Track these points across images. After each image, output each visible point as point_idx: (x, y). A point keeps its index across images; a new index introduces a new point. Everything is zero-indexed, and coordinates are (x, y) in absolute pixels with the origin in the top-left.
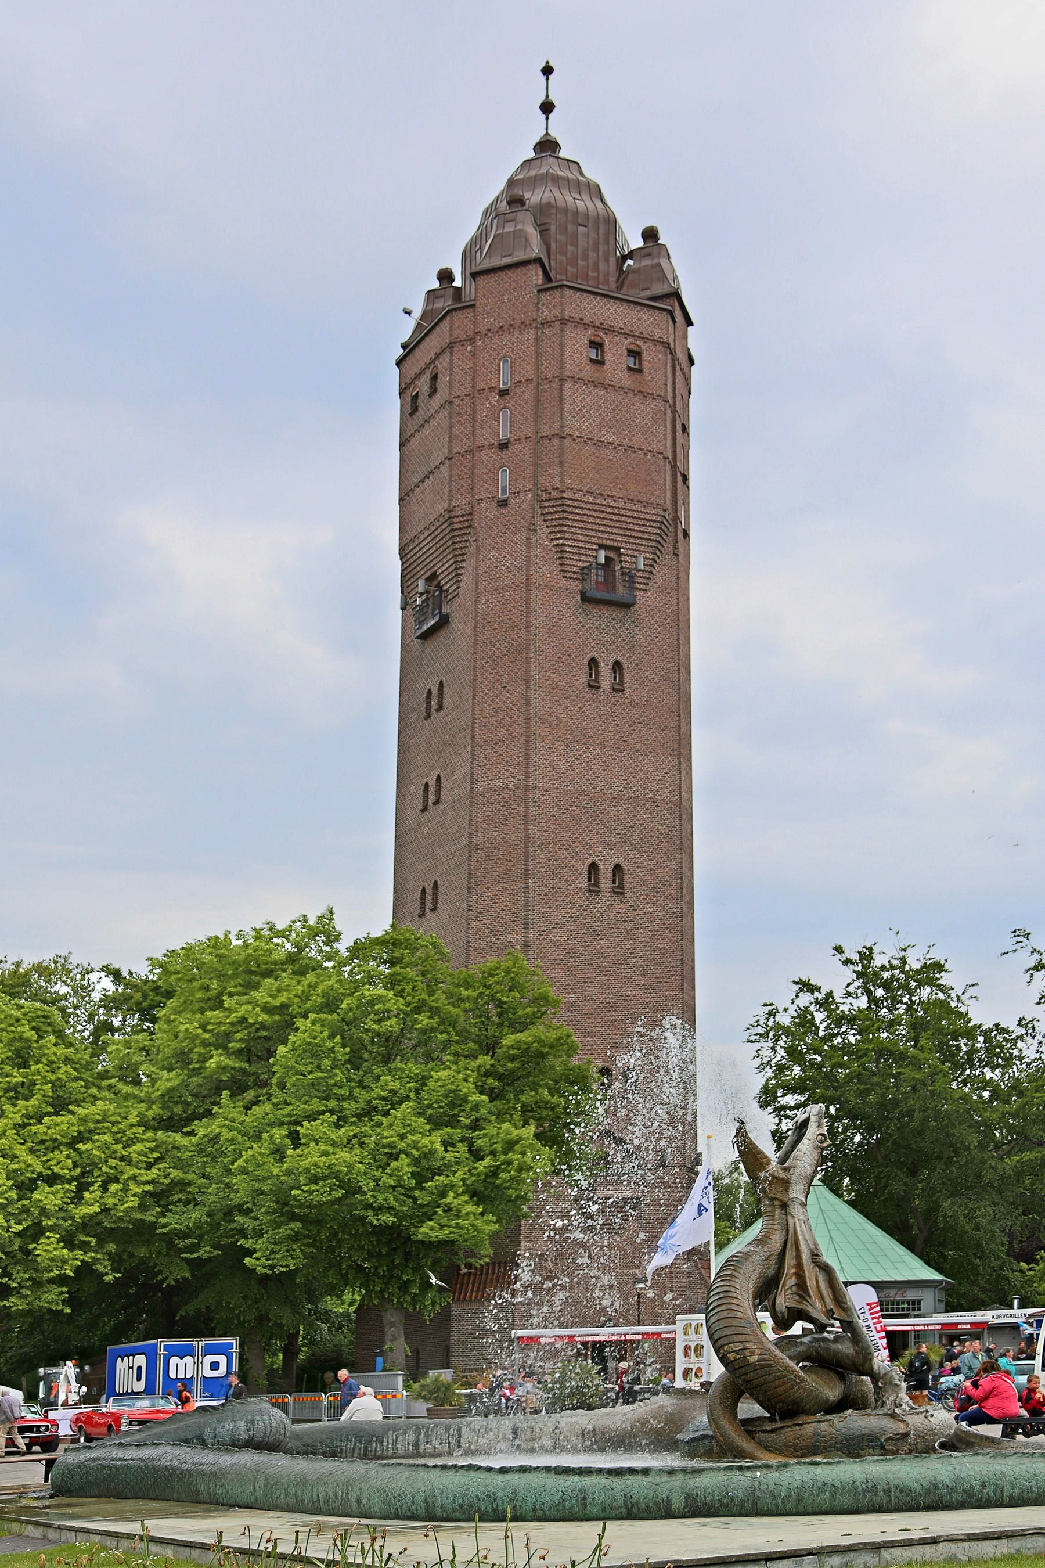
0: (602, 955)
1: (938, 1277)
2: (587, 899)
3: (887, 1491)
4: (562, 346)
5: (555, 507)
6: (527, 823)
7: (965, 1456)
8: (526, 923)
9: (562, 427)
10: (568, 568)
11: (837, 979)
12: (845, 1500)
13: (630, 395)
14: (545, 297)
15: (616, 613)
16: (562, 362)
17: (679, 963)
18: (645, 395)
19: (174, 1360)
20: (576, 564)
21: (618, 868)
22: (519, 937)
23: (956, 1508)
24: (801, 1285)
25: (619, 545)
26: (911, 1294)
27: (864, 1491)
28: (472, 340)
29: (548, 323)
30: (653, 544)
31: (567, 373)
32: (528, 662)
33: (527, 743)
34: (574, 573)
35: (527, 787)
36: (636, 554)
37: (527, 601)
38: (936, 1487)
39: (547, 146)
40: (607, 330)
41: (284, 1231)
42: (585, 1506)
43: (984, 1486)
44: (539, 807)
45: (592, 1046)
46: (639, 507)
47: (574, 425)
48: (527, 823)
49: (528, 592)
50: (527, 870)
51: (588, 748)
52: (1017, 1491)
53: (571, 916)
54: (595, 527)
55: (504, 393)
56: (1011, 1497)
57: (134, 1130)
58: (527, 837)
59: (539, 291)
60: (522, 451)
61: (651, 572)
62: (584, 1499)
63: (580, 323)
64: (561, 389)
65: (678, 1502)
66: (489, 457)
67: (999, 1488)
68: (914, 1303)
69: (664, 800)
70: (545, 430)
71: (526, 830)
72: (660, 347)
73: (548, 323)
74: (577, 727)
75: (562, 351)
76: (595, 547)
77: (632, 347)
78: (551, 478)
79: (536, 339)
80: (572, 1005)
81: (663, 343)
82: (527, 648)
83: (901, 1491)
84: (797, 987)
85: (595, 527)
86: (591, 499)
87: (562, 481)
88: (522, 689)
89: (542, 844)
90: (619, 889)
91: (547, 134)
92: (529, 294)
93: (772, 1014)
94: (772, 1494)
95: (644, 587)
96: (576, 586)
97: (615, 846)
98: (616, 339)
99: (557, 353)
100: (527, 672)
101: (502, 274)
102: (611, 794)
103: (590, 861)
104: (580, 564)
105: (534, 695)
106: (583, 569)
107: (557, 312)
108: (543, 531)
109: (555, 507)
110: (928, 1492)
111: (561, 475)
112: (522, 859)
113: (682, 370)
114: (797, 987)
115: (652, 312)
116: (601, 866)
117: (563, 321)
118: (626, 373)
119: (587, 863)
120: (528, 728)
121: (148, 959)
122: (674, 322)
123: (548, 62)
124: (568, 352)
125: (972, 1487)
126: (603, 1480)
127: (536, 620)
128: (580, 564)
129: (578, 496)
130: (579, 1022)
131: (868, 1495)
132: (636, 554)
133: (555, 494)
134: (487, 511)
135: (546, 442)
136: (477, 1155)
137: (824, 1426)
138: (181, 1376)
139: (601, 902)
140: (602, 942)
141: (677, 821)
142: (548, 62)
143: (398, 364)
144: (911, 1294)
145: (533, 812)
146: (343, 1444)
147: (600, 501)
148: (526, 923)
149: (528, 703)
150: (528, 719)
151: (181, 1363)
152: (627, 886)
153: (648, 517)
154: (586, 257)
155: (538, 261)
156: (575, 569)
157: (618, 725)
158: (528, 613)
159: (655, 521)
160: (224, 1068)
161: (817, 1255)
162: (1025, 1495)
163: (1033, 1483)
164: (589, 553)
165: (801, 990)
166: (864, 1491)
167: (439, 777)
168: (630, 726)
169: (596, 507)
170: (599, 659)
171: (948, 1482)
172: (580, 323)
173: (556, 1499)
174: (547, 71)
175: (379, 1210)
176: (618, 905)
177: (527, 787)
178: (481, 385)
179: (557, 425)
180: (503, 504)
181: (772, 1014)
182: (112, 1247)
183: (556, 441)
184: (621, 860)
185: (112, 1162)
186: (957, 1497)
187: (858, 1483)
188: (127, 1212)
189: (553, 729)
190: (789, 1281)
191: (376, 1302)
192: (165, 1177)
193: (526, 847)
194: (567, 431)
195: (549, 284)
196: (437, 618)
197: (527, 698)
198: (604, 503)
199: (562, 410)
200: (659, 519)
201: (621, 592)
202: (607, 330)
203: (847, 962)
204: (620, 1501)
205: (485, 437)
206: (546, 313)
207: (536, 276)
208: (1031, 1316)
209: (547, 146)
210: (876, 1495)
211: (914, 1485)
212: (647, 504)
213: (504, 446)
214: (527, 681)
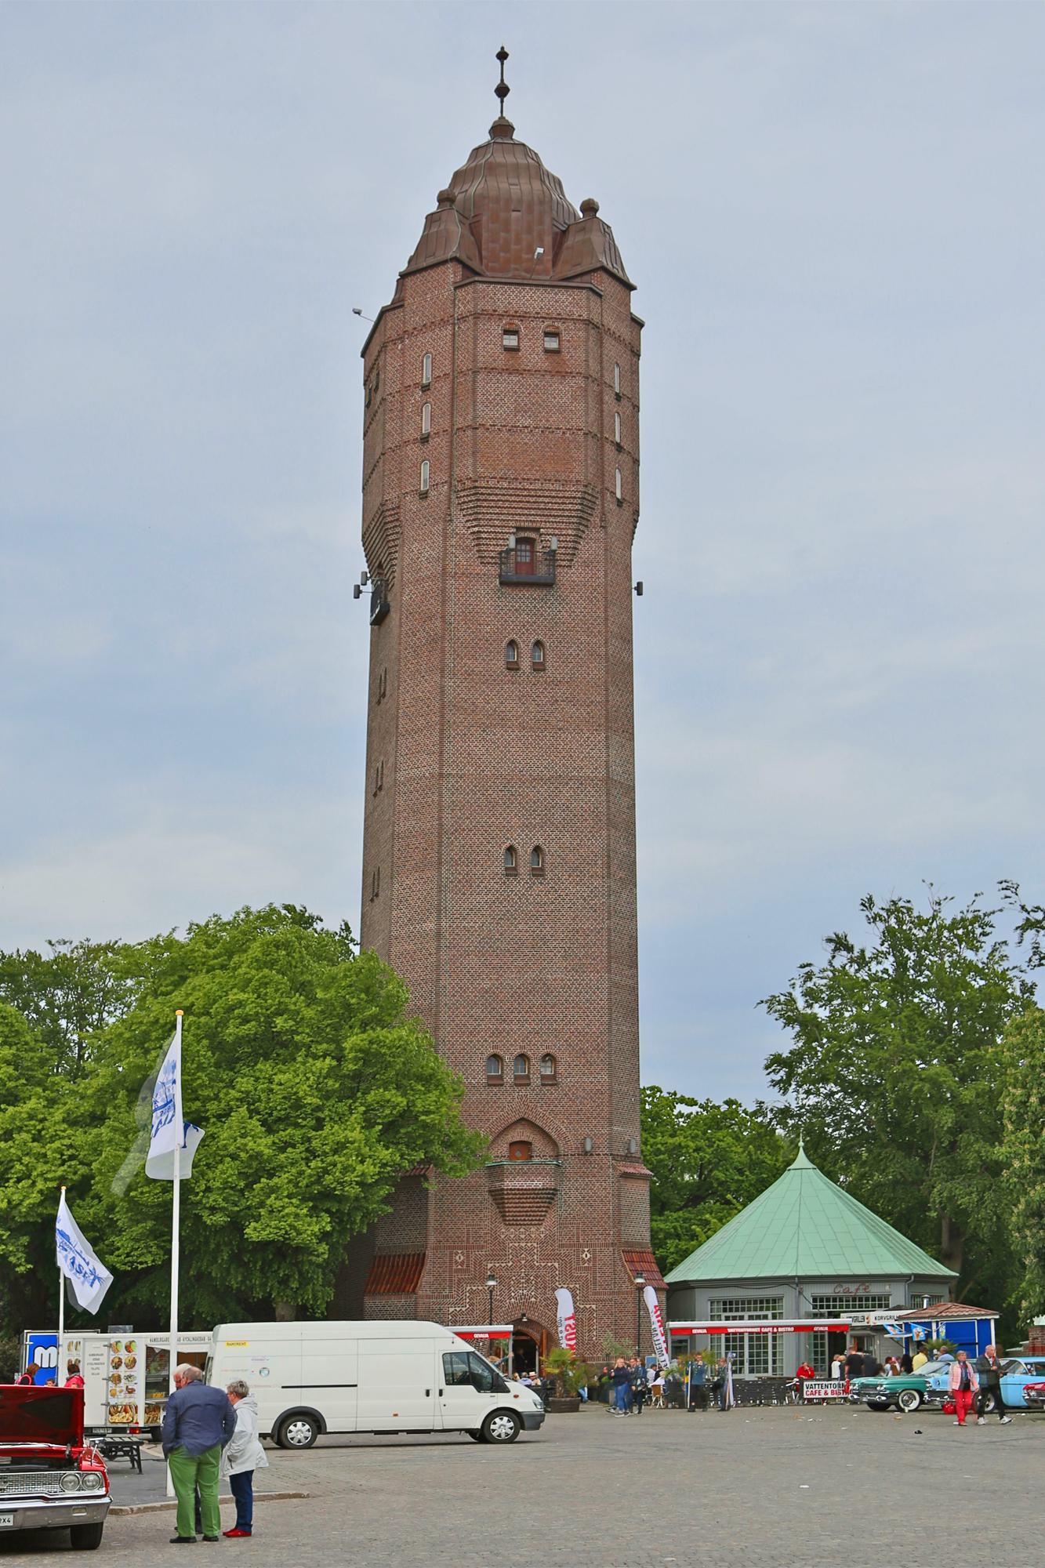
1: (943, 1270)
4: (475, 339)
5: (471, 495)
6: (440, 811)
8: (439, 911)
9: (474, 418)
11: (868, 938)
13: (548, 377)
14: (460, 293)
15: (536, 593)
16: (475, 355)
18: (563, 375)
19: (39, 1351)
20: (493, 549)
21: (537, 850)
22: (432, 926)
26: (876, 1289)
28: (402, 339)
29: (463, 318)
31: (480, 365)
32: (443, 651)
33: (442, 731)
35: (441, 775)
37: (443, 590)
39: (502, 129)
40: (523, 317)
41: (137, 1230)
46: (557, 486)
47: (487, 415)
48: (440, 811)
49: (444, 581)
50: (440, 859)
54: (512, 511)
55: (426, 388)
57: (57, 1127)
58: (440, 825)
59: (456, 288)
60: (439, 443)
63: (492, 315)
64: (474, 381)
66: (413, 451)
68: (841, 1300)
70: (460, 422)
71: (440, 818)
73: (463, 318)
75: (475, 344)
78: (466, 468)
79: (453, 335)
82: (443, 637)
84: (832, 946)
85: (512, 511)
86: (506, 485)
87: (475, 471)
88: (437, 679)
90: (538, 873)
91: (502, 118)
92: (447, 291)
93: (809, 977)
96: (494, 570)
98: (533, 324)
99: (471, 347)
100: (442, 660)
101: (425, 274)
105: (449, 683)
106: (500, 553)
107: (470, 307)
108: (460, 521)
109: (471, 495)
111: (474, 465)
112: (436, 848)
114: (832, 946)
115: (570, 291)
117: (476, 316)
118: (542, 356)
119: (504, 847)
120: (442, 716)
124: (481, 345)
127: (451, 608)
133: (468, 484)
134: (412, 504)
135: (461, 433)
136: (312, 1154)
138: (45, 1365)
139: (518, 886)
141: (604, 798)
144: (876, 1289)
145: (447, 799)
148: (439, 911)
149: (442, 692)
150: (443, 707)
151: (46, 1353)
152: (548, 867)
153: (567, 494)
154: (518, 241)
155: (455, 259)
158: (444, 603)
165: (835, 950)
172: (492, 315)
174: (502, 56)
175: (213, 1210)
176: (538, 888)
177: (441, 775)
178: (408, 382)
179: (470, 417)
180: (424, 496)
181: (809, 977)
182: (25, 1240)
183: (469, 432)
184: (541, 842)
185: (26, 1160)
188: (32, 1207)
192: (75, 1173)
193: (440, 836)
194: (480, 421)
195: (470, 273)
197: (442, 687)
199: (475, 402)
201: (542, 571)
202: (523, 317)
203: (876, 918)
205: (411, 434)
206: (461, 309)
207: (452, 273)
208: (900, 1318)
209: (502, 129)
212: (566, 483)
213: (425, 440)
214: (442, 671)
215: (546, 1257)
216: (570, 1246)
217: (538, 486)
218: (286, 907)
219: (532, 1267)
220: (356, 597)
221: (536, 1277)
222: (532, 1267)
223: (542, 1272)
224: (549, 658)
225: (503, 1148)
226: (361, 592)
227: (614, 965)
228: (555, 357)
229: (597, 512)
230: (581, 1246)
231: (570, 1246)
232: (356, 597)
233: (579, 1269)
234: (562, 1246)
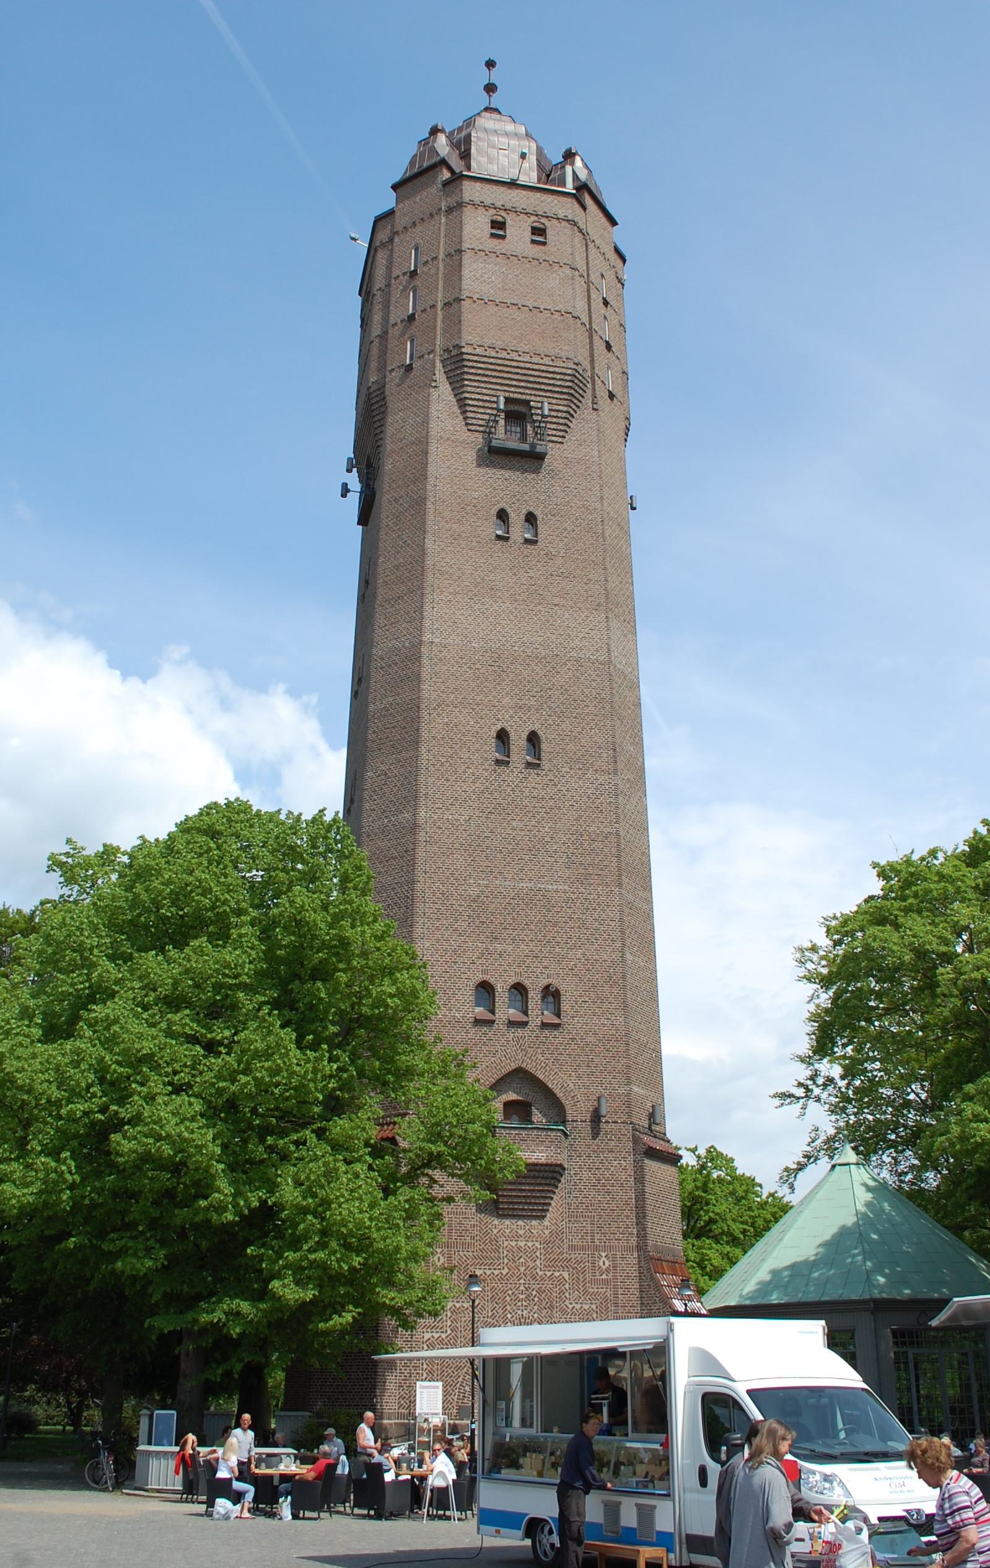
0: (514, 839)
2: (495, 771)
17: (614, 851)
25: (528, 398)
34: (480, 426)
44: (436, 664)
45: (500, 955)
51: (496, 602)
53: (474, 792)
69: (589, 659)
72: (564, 224)
74: (483, 579)
77: (536, 224)
80: (474, 901)
81: (568, 221)
86: (494, 354)
89: (439, 706)
95: (560, 440)
97: (529, 709)
102: (524, 652)
121: (69, 841)
122: (584, 209)
123: (875, 865)
128: (487, 417)
129: (479, 351)
130: (483, 923)
140: (514, 824)
142: (875, 865)
147: (504, 354)
156: (480, 422)
157: (531, 578)
159: (565, 374)
160: (299, 923)
168: (547, 579)
169: (499, 362)
170: (509, 510)
184: (536, 727)
189: (455, 581)
198: (508, 357)
215: (551, 1264)
216: (583, 1248)
217: (527, 358)
218: (911, 1468)
219: (534, 1278)
220: (344, 495)
221: (540, 1291)
222: (534, 1278)
223: (548, 1285)
224: (154, 1506)
225: (498, 1105)
226: (348, 491)
227: (625, 879)
228: (542, 247)
229: (589, 392)
230: (596, 1248)
231: (583, 1248)
232: (344, 495)
233: (596, 1282)
234: (572, 1248)
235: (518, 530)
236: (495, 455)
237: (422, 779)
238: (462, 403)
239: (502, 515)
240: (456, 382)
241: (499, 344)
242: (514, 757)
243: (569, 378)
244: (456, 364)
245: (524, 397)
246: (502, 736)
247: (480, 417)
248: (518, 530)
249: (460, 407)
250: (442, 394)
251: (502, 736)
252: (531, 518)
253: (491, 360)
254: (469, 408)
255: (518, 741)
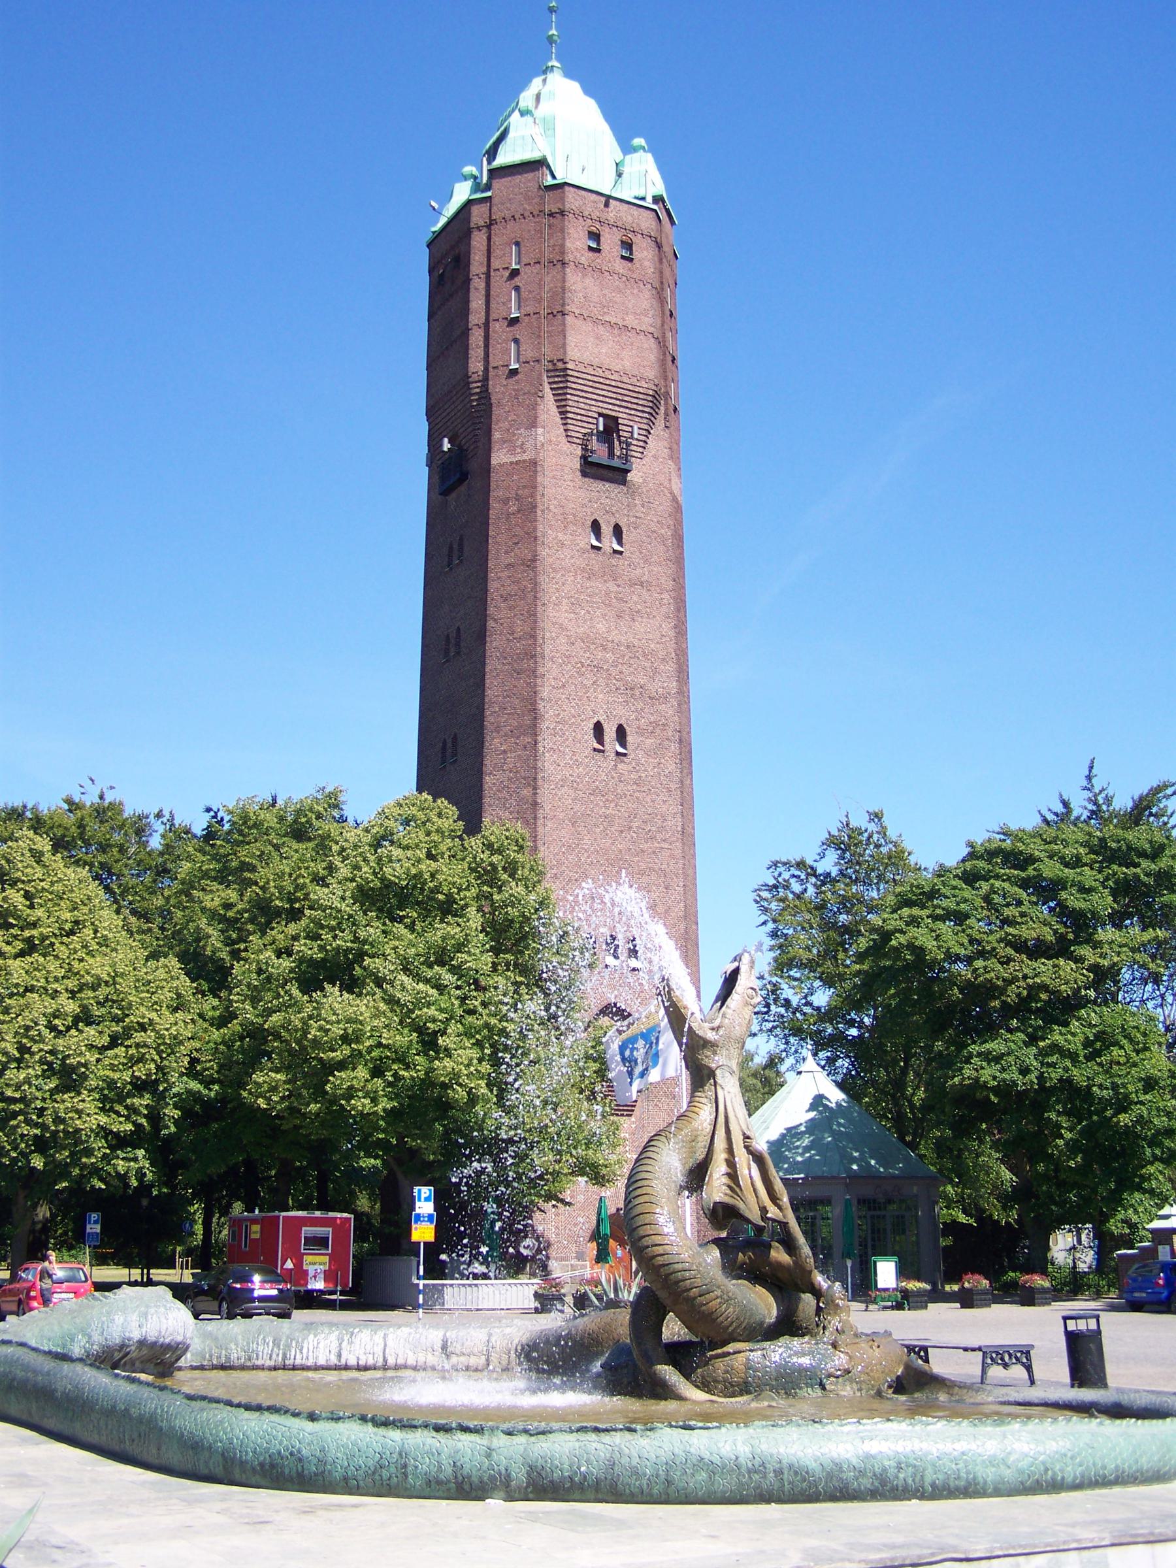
3: (779, 1472)
7: (876, 1423)
10: (573, 434)
12: (723, 1484)
23: (864, 1500)
24: (733, 1175)
27: (749, 1472)
30: (646, 415)
36: (631, 423)
38: (841, 1470)
42: (405, 1475)
43: (899, 1468)
52: (941, 1477)
56: (933, 1485)
61: (645, 442)
62: (405, 1466)
65: (519, 1476)
67: (919, 1472)
76: (596, 415)
83: (796, 1473)
94: (635, 1473)
103: (595, 720)
104: (583, 430)
110: (830, 1476)
113: (669, 262)
116: (605, 726)
125: (885, 1470)
126: (429, 1441)
128: (583, 430)
131: (756, 1477)
132: (631, 423)
137: (756, 1356)
143: (428, 246)
146: (260, 1348)
161: (748, 1138)
162: (952, 1484)
163: (961, 1465)
164: (591, 420)
166: (749, 1472)
167: (459, 629)
171: (854, 1461)
173: (371, 1463)
186: (866, 1483)
187: (742, 1460)
190: (718, 1170)
191: (273, 1172)
196: (458, 475)
200: (651, 392)
204: (448, 1471)
210: (765, 1477)
211: (813, 1465)
235: (611, 744)
236: (591, 468)
237: (472, 256)
238: (563, 414)
239: (596, 527)
240: (561, 397)
241: (595, 362)
242: (608, 747)
243: (650, 398)
244: (560, 373)
245: (613, 414)
246: (598, 729)
247: (578, 431)
248: (611, 744)
249: (560, 413)
250: (548, 406)
251: (598, 729)
252: (621, 733)
253: (589, 377)
254: (570, 421)
255: (610, 733)
